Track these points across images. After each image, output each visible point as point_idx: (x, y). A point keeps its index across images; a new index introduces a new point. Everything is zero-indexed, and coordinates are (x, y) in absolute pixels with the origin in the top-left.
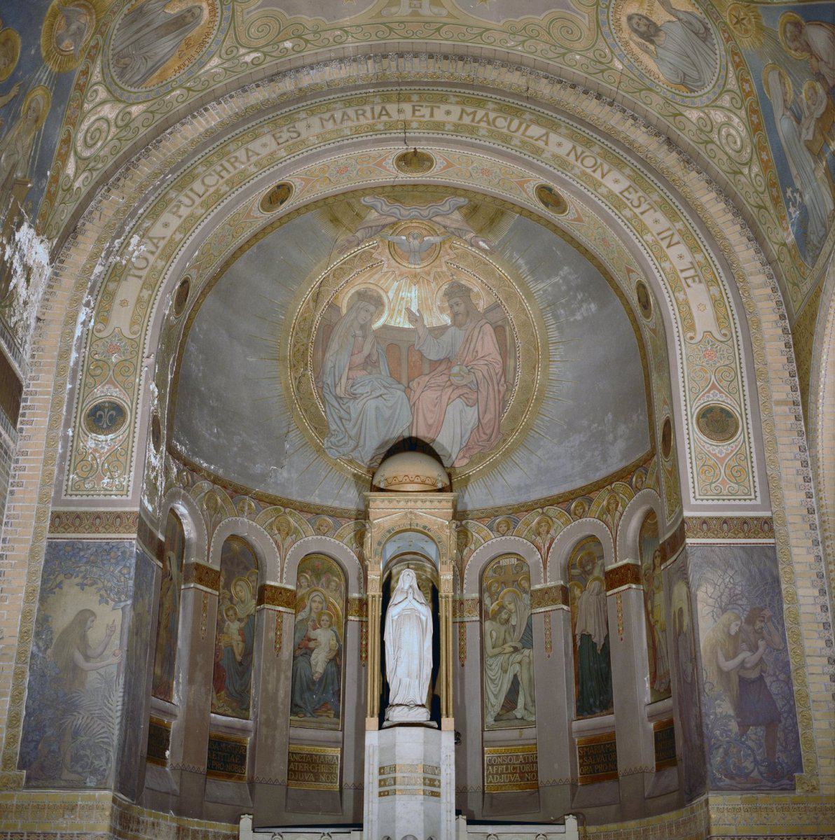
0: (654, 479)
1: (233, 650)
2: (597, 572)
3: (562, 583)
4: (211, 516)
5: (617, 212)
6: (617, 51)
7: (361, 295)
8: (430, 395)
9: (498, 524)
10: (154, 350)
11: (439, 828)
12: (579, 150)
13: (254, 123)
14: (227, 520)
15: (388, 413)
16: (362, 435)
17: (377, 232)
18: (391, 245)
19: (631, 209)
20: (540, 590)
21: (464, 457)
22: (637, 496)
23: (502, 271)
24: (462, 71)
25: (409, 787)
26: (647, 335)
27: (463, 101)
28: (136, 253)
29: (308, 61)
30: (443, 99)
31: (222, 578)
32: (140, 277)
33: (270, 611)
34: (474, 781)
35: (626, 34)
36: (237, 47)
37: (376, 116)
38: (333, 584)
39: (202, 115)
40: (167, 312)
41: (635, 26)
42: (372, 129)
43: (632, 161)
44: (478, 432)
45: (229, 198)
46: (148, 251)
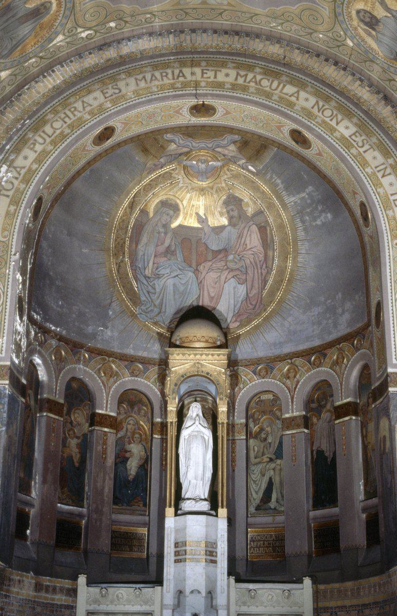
0: (369, 342)
1: (73, 460)
2: (328, 406)
3: (304, 413)
4: (56, 367)
5: (347, 151)
6: (349, 33)
7: (164, 204)
8: (213, 275)
9: (260, 370)
10: (19, 250)
11: (216, 585)
12: (321, 104)
13: (88, 82)
14: (68, 367)
15: (182, 288)
16: (164, 305)
17: (175, 158)
18: (185, 168)
19: (357, 149)
20: (289, 418)
21: (236, 321)
22: (357, 354)
23: (265, 188)
24: (237, 44)
25: (195, 557)
26: (366, 239)
27: (239, 66)
28: (5, 179)
29: (127, 35)
30: (224, 65)
31: (65, 408)
32: (8, 196)
33: (99, 432)
34: (240, 553)
35: (355, 22)
36: (76, 28)
37: (176, 78)
38: (143, 411)
39: (50, 75)
40: (27, 221)
41: (362, 18)
42: (173, 87)
43: (359, 112)
44: (247, 302)
45: (71, 138)
46: (13, 177)
